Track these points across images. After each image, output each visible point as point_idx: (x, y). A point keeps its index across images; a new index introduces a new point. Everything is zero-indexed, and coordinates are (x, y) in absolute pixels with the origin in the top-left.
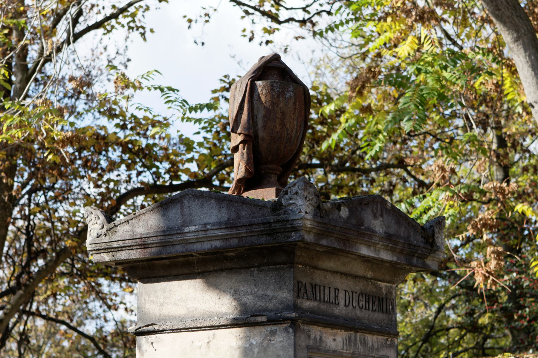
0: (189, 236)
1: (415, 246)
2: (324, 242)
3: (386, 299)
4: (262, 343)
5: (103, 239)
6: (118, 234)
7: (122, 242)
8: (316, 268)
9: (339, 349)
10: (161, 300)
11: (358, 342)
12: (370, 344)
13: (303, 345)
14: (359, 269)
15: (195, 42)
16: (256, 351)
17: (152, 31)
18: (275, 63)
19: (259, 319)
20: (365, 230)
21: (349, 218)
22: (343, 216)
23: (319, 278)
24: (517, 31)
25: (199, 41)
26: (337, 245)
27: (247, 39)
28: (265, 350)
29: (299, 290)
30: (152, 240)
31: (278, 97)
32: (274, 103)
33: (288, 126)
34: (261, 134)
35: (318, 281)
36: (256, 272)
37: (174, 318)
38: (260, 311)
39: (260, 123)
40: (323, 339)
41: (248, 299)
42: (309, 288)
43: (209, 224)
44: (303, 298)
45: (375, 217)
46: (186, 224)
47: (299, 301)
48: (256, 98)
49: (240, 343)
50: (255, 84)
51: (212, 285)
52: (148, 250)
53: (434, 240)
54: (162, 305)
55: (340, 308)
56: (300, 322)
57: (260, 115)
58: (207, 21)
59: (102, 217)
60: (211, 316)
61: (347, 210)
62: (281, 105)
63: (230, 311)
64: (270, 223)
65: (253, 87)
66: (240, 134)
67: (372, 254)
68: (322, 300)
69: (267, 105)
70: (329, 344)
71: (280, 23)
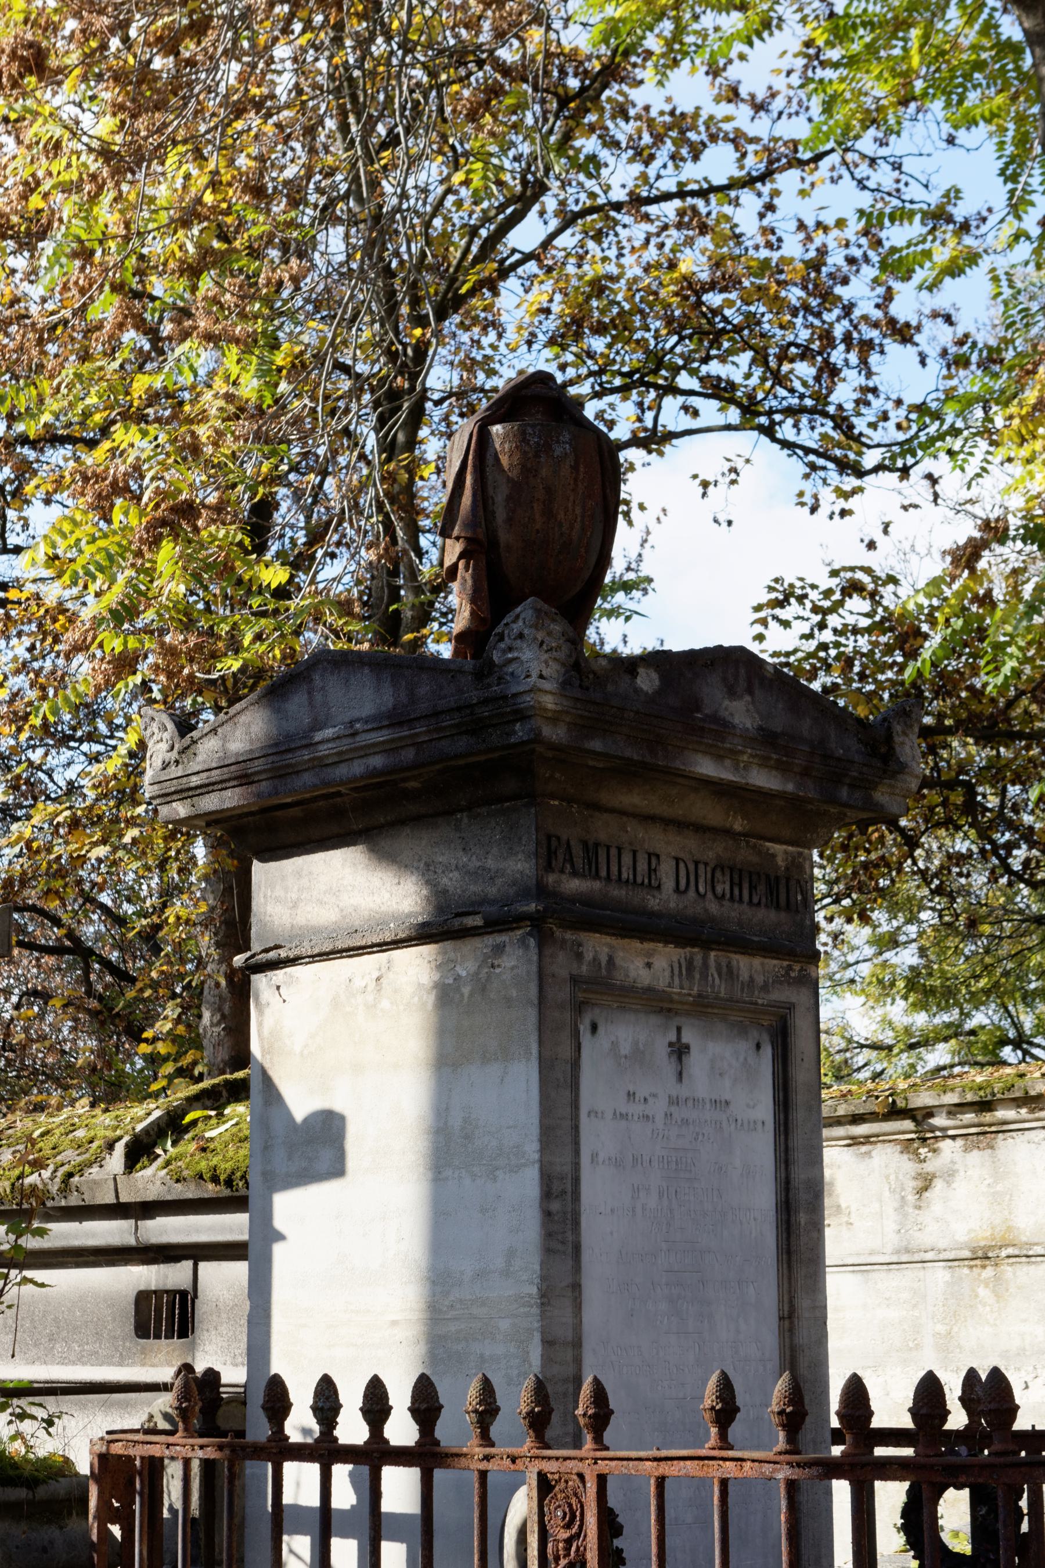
0: (324, 750)
1: (839, 759)
3: (788, 880)
4: (477, 973)
5: (175, 771)
6: (200, 758)
7: (204, 775)
8: (597, 807)
9: (662, 984)
10: (294, 896)
11: (713, 970)
12: (744, 976)
13: (564, 973)
14: (706, 810)
15: (716, 521)
16: (466, 990)
17: (642, 507)
18: (538, 389)
20: (702, 720)
21: (659, 692)
22: (645, 688)
23: (604, 829)
25: (722, 519)
26: (631, 753)
27: (806, 510)
28: (484, 989)
29: (551, 855)
30: (257, 765)
31: (537, 455)
32: (528, 469)
33: (561, 516)
34: (504, 536)
35: (603, 836)
36: (466, 820)
37: (316, 930)
38: (473, 904)
39: (501, 515)
40: (618, 961)
41: (451, 881)
42: (577, 851)
43: (358, 720)
44: (562, 871)
45: (732, 693)
46: (317, 725)
47: (551, 879)
48: (490, 461)
49: (436, 976)
50: (489, 433)
51: (385, 854)
52: (253, 788)
53: (891, 749)
54: (295, 905)
55: (664, 896)
56: (551, 925)
57: (500, 496)
58: (733, 482)
59: (170, 726)
60: (382, 923)
61: (654, 676)
62: (544, 472)
63: (418, 909)
64: (471, 706)
65: (483, 437)
66: (457, 538)
68: (614, 877)
69: (514, 474)
70: (633, 974)
71: (860, 474)
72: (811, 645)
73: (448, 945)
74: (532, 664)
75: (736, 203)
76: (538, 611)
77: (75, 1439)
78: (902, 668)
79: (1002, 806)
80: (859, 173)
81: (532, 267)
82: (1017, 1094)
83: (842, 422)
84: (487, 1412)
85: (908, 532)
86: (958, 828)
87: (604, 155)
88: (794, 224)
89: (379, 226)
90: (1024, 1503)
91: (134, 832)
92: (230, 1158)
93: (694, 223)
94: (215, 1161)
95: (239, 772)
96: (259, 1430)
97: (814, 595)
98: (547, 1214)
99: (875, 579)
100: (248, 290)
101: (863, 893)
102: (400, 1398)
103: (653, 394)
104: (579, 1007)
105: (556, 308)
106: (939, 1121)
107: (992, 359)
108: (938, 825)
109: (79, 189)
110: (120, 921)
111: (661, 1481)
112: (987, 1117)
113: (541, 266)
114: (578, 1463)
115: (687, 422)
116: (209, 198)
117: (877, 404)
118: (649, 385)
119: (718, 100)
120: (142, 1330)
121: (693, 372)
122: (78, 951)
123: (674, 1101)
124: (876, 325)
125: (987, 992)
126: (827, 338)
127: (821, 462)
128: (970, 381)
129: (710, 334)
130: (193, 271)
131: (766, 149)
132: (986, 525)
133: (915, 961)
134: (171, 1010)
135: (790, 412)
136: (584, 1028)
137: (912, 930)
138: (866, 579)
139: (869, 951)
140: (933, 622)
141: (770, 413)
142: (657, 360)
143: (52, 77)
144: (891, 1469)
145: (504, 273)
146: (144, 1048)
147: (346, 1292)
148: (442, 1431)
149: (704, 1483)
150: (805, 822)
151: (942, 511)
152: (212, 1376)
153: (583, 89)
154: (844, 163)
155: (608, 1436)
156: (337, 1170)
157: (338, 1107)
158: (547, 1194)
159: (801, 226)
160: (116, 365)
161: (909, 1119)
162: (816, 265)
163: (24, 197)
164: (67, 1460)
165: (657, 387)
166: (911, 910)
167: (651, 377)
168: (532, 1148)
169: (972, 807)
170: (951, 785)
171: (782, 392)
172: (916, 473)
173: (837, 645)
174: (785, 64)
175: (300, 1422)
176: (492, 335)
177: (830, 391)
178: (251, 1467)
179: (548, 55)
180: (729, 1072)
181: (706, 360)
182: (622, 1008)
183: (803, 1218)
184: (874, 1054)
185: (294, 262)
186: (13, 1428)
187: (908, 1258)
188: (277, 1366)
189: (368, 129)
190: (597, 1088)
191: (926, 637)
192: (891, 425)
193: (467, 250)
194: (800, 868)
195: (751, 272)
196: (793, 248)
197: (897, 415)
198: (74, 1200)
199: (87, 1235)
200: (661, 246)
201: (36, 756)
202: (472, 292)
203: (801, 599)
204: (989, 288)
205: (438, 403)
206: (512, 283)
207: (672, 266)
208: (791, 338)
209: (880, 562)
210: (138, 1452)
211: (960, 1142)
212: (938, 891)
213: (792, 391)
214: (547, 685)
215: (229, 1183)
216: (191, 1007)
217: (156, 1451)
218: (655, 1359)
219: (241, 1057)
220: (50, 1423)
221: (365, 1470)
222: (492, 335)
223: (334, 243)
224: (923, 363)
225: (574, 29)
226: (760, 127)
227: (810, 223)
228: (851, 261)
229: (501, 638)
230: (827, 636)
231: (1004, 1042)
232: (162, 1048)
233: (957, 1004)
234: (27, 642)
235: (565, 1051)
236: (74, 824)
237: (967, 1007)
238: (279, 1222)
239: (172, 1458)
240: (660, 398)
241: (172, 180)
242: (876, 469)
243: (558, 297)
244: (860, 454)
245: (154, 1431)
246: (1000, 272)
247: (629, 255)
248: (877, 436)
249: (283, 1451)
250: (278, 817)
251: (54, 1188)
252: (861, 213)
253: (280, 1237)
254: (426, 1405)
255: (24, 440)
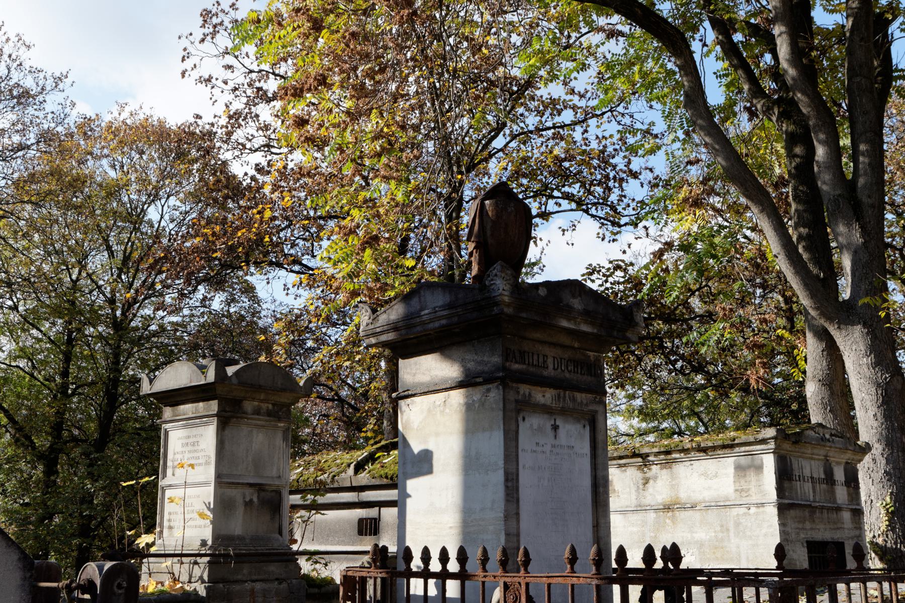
0: (425, 318)
2: (524, 315)
5: (371, 327)
9: (549, 403)
12: (579, 400)
14: (565, 340)
16: (477, 405)
17: (541, 239)
19: (478, 380)
24: (762, 205)
25: (570, 242)
30: (400, 324)
34: (490, 241)
37: (422, 384)
39: (489, 233)
41: (471, 365)
42: (517, 354)
45: (574, 297)
46: (422, 309)
47: (508, 364)
54: (414, 375)
57: (489, 226)
59: (369, 310)
60: (445, 380)
65: (482, 205)
67: (572, 326)
71: (620, 226)
72: (602, 289)
73: (470, 389)
74: (500, 286)
75: (574, 130)
76: (502, 266)
77: (335, 572)
78: (636, 296)
79: (673, 346)
80: (618, 119)
81: (501, 154)
82: (680, 448)
83: (613, 208)
84: (485, 560)
85: (638, 247)
86: (657, 354)
87: (526, 114)
88: (594, 137)
89: (445, 140)
90: (684, 596)
91: (360, 356)
92: (392, 470)
93: (558, 137)
94: (386, 471)
95: (394, 327)
96: (401, 567)
97: (603, 270)
98: (507, 487)
99: (626, 264)
100: (399, 161)
101: (622, 379)
102: (453, 554)
103: (544, 199)
104: (518, 411)
105: (509, 168)
106: (651, 458)
107: (667, 184)
108: (650, 353)
109: (339, 126)
110: (355, 389)
111: (549, 585)
112: (669, 457)
113: (504, 154)
114: (518, 578)
115: (556, 208)
116: (385, 130)
117: (625, 201)
118: (543, 195)
119: (567, 94)
120: (360, 533)
121: (559, 191)
122: (341, 401)
123: (553, 446)
124: (625, 172)
125: (668, 414)
126: (607, 177)
127: (606, 222)
128: (659, 192)
129: (565, 177)
130: (379, 155)
131: (584, 110)
132: (666, 243)
133: (641, 403)
134: (373, 421)
135: (595, 204)
136: (520, 419)
137: (640, 392)
138: (622, 264)
139: (624, 400)
140: (646, 278)
141: (587, 204)
142: (546, 186)
143: (329, 87)
144: (635, 582)
145: (491, 156)
146: (363, 434)
147: (433, 516)
148: (469, 567)
149: (565, 586)
150: (601, 344)
151: (648, 241)
152: (385, 548)
153: (518, 90)
154: (613, 115)
155: (529, 568)
156: (430, 471)
157: (430, 448)
158: (507, 480)
159: (597, 137)
160: (353, 189)
161: (641, 458)
162: (603, 152)
163: (318, 129)
164: (332, 579)
165: (546, 196)
166: (640, 386)
167: (544, 192)
168: (501, 463)
169: (661, 347)
170: (654, 338)
171: (591, 197)
172: (641, 225)
173: (612, 288)
174: (591, 81)
175: (416, 564)
176: (487, 177)
177: (609, 197)
178: (399, 580)
179: (506, 78)
180: (574, 436)
181: (563, 186)
182: (534, 412)
183: (601, 490)
184: (627, 438)
185: (415, 151)
186: (313, 567)
187: (640, 509)
188: (408, 543)
189: (442, 104)
190: (525, 440)
191: (644, 285)
192: (630, 209)
193: (477, 148)
194: (599, 361)
195: (579, 154)
196: (594, 145)
197: (633, 205)
198: (336, 485)
199: (341, 498)
200: (547, 146)
201: (324, 330)
202: (479, 163)
203: (599, 272)
204: (665, 157)
205: (467, 202)
206: (494, 159)
207: (551, 152)
208: (594, 177)
209: (627, 258)
210: (357, 575)
211: (659, 466)
212: (650, 377)
213: (595, 197)
214: (506, 293)
215: (392, 479)
216: (380, 420)
217: (364, 574)
218: (548, 541)
219: (395, 431)
220: (326, 565)
221: (440, 581)
222: (487, 177)
223: (430, 146)
224: (642, 186)
225: (515, 70)
226: (582, 103)
227: (600, 136)
228: (615, 150)
229: (489, 276)
230: (608, 285)
231: (674, 433)
232: (369, 434)
233: (657, 419)
234: (321, 289)
235: (513, 427)
236: (338, 353)
237: (661, 420)
238: (409, 491)
239: (370, 577)
240: (547, 200)
241: (371, 124)
242: (626, 224)
243: (510, 164)
244: (620, 219)
245: (364, 567)
246: (669, 151)
247: (536, 149)
248: (626, 213)
249: (410, 574)
250: (408, 342)
251: (329, 481)
252: (619, 131)
253: (409, 496)
254: (462, 557)
255: (320, 218)
